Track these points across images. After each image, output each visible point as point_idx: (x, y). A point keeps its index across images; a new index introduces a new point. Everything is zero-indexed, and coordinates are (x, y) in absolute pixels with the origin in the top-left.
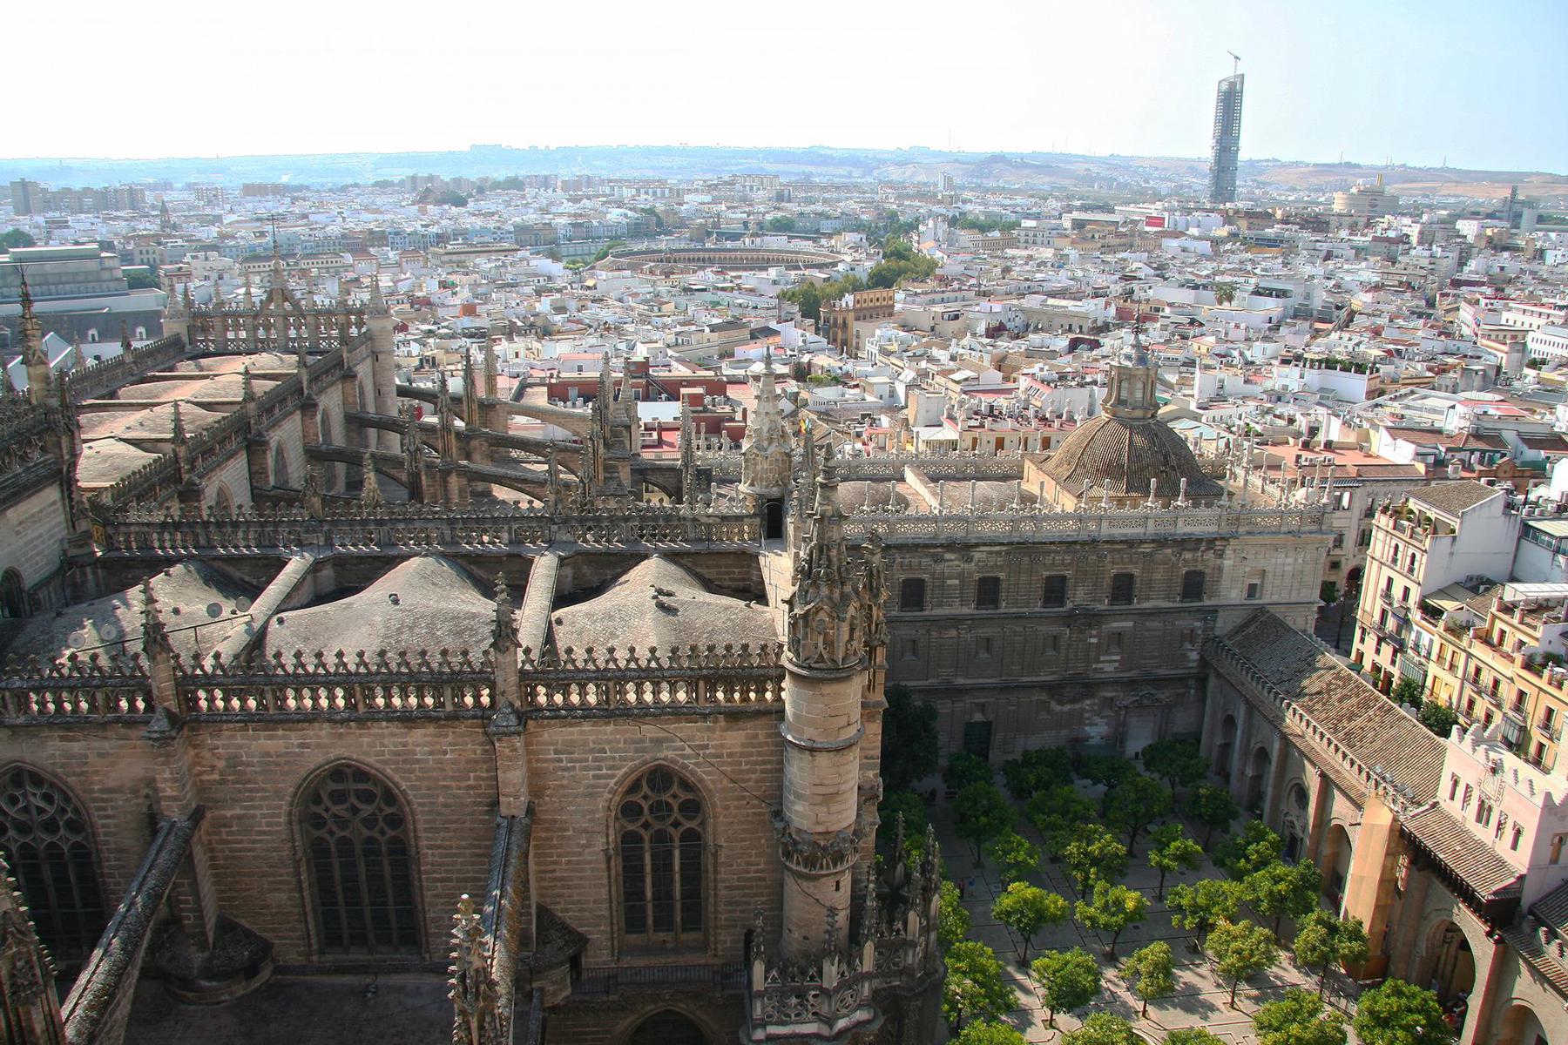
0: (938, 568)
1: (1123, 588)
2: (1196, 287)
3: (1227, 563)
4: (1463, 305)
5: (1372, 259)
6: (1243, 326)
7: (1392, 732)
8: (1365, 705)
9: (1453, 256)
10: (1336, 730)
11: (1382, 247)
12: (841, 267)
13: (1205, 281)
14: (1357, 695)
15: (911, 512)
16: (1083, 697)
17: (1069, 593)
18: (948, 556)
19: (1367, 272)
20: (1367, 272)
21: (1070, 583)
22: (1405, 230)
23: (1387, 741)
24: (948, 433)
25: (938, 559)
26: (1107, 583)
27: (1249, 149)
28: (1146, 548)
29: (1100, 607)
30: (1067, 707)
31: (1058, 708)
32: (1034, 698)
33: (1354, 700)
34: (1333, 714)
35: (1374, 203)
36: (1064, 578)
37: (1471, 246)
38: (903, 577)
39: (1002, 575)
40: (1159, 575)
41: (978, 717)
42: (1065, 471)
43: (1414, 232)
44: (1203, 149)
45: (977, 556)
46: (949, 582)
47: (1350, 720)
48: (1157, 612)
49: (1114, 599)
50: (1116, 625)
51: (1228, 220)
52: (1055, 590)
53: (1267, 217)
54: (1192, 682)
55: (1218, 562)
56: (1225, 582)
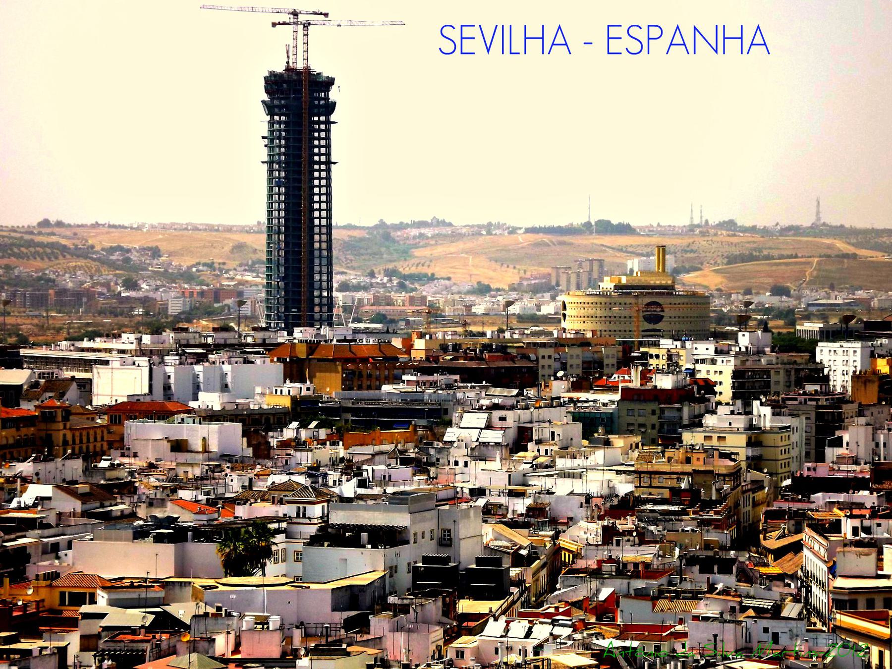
4: (807, 535)
5: (618, 442)
6: (274, 622)
9: (799, 425)
11: (645, 412)
19: (601, 472)
20: (601, 472)
22: (704, 372)
27: (357, 197)
35: (655, 307)
37: (841, 400)
43: (722, 374)
44: (239, 198)
51: (295, 370)
53: (390, 365)
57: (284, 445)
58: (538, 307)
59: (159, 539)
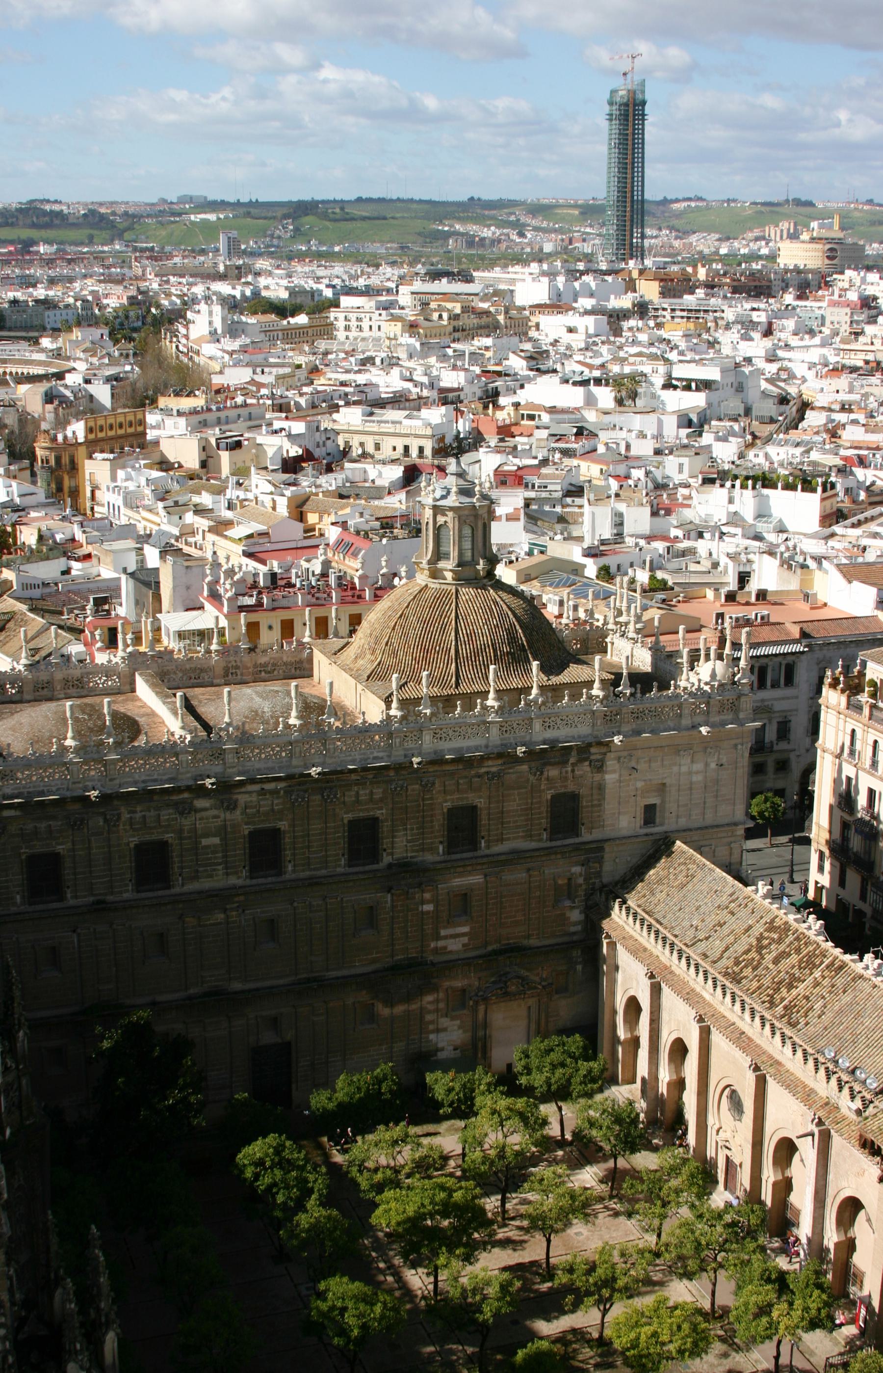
0: (187, 822)
1: (463, 828)
2: (585, 383)
3: (610, 778)
7: (846, 998)
8: (809, 963)
10: (772, 1004)
12: (70, 379)
13: (597, 373)
14: (798, 951)
15: (141, 741)
16: (421, 991)
17: (386, 843)
18: (200, 803)
21: (385, 827)
23: (840, 1011)
24: (209, 617)
25: (185, 809)
26: (438, 822)
28: (493, 766)
29: (429, 857)
30: (399, 1009)
31: (385, 1012)
32: (350, 1001)
33: (794, 959)
34: (767, 981)
36: (375, 820)
38: (134, 840)
39: (283, 825)
40: (514, 804)
41: (269, 1038)
42: (367, 665)
44: (596, 181)
45: (242, 799)
46: (205, 842)
47: (790, 987)
48: (516, 857)
49: (452, 846)
50: (458, 882)
52: (364, 839)
54: (576, 953)
55: (597, 777)
56: (610, 806)
57: (630, 329)
58: (759, 250)
59: (575, 384)
